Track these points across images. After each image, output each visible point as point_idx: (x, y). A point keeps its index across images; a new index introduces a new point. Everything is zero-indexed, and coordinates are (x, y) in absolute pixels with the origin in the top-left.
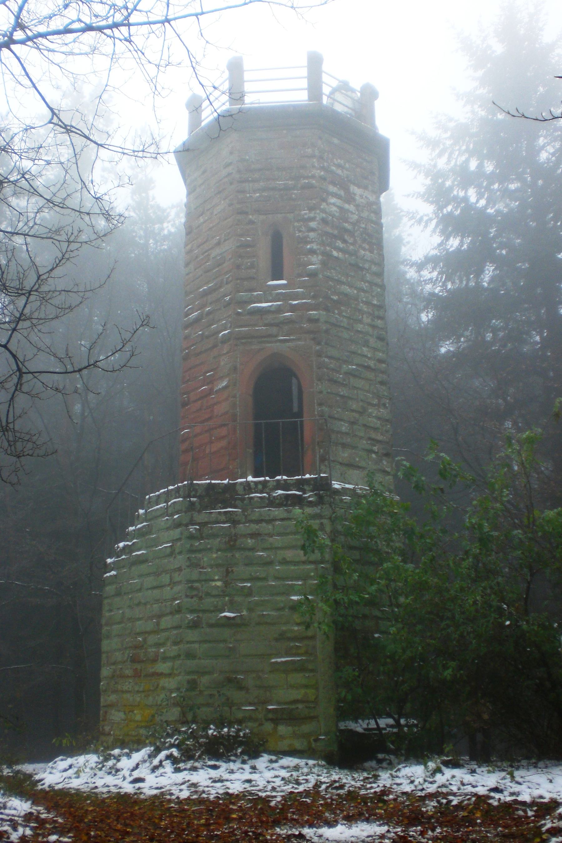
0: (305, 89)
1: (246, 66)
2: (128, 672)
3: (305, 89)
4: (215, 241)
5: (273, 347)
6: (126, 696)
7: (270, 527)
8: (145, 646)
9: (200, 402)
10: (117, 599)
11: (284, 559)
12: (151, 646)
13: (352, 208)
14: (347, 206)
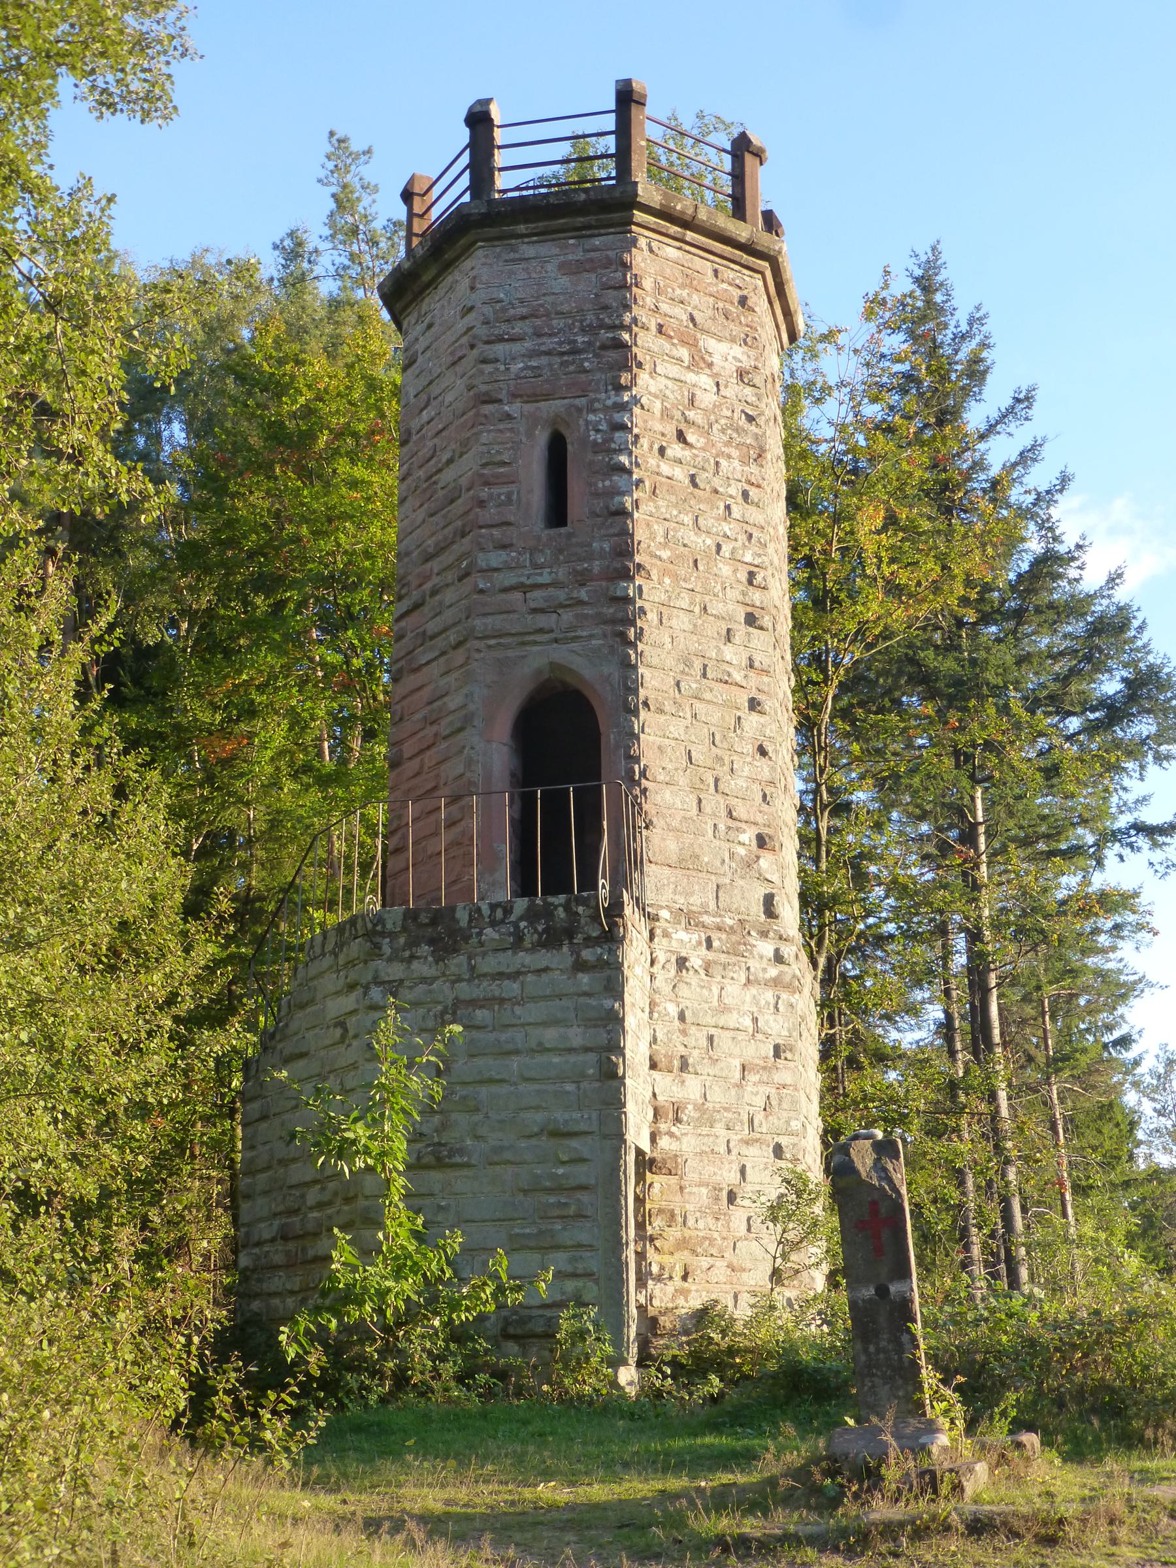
0: (500, 147)
1: (497, 114)
2: (278, 1259)
3: (500, 147)
4: (445, 457)
5: (561, 654)
6: (276, 1302)
7: (515, 986)
8: (304, 1209)
9: (417, 760)
10: (264, 1125)
11: (540, 1044)
12: (311, 1208)
13: (704, 380)
14: (690, 377)
